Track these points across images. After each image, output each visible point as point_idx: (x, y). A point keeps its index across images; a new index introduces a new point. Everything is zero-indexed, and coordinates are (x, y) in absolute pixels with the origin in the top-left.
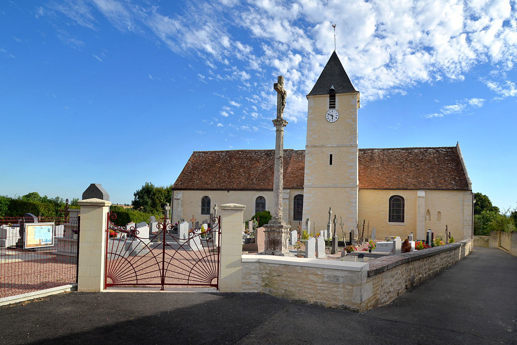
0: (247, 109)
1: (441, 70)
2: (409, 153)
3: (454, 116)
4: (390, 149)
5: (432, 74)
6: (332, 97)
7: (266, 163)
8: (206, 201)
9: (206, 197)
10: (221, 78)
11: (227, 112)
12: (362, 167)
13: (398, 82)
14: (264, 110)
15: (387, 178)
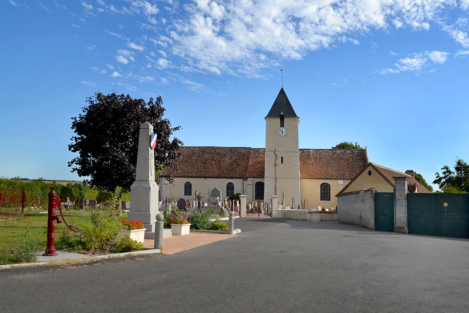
0: (153, 54)
1: (399, 14)
2: (334, 153)
3: (410, 75)
4: (321, 150)
5: (389, 19)
6: (282, 118)
7: (231, 158)
8: (188, 185)
9: (188, 182)
10: (115, 10)
11: (125, 57)
12: (302, 162)
13: (346, 27)
14: (176, 56)
15: (319, 171)
